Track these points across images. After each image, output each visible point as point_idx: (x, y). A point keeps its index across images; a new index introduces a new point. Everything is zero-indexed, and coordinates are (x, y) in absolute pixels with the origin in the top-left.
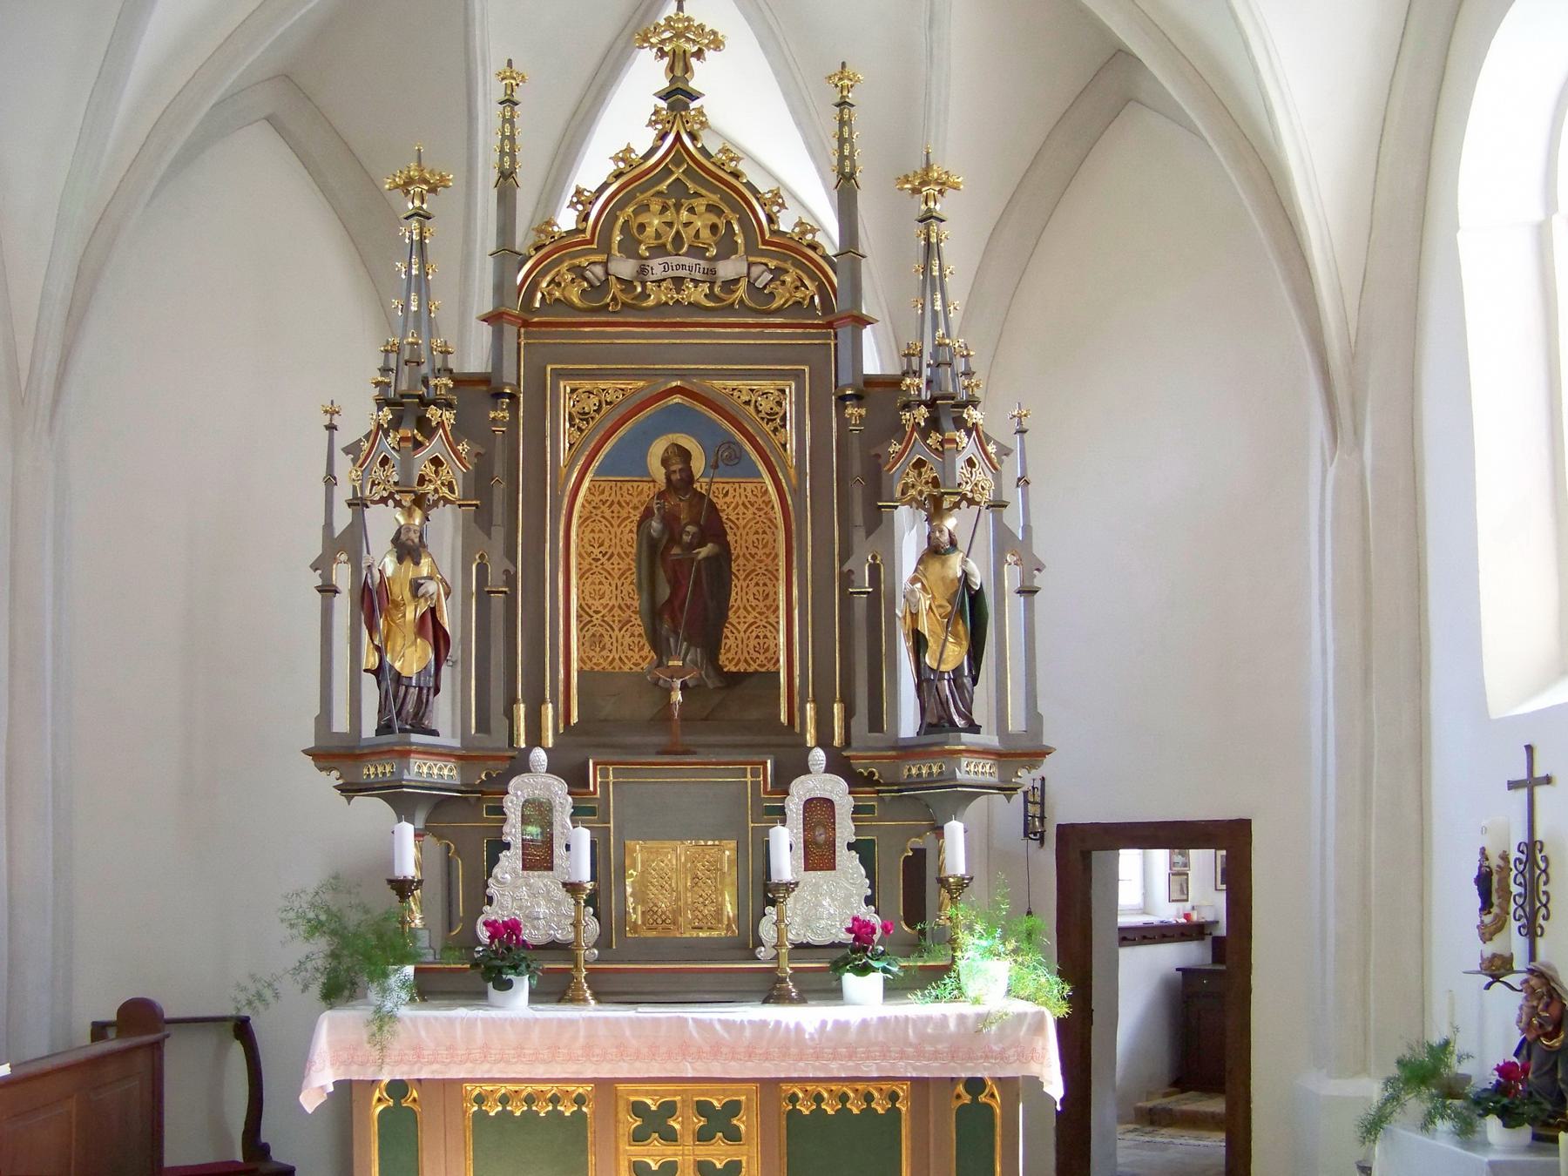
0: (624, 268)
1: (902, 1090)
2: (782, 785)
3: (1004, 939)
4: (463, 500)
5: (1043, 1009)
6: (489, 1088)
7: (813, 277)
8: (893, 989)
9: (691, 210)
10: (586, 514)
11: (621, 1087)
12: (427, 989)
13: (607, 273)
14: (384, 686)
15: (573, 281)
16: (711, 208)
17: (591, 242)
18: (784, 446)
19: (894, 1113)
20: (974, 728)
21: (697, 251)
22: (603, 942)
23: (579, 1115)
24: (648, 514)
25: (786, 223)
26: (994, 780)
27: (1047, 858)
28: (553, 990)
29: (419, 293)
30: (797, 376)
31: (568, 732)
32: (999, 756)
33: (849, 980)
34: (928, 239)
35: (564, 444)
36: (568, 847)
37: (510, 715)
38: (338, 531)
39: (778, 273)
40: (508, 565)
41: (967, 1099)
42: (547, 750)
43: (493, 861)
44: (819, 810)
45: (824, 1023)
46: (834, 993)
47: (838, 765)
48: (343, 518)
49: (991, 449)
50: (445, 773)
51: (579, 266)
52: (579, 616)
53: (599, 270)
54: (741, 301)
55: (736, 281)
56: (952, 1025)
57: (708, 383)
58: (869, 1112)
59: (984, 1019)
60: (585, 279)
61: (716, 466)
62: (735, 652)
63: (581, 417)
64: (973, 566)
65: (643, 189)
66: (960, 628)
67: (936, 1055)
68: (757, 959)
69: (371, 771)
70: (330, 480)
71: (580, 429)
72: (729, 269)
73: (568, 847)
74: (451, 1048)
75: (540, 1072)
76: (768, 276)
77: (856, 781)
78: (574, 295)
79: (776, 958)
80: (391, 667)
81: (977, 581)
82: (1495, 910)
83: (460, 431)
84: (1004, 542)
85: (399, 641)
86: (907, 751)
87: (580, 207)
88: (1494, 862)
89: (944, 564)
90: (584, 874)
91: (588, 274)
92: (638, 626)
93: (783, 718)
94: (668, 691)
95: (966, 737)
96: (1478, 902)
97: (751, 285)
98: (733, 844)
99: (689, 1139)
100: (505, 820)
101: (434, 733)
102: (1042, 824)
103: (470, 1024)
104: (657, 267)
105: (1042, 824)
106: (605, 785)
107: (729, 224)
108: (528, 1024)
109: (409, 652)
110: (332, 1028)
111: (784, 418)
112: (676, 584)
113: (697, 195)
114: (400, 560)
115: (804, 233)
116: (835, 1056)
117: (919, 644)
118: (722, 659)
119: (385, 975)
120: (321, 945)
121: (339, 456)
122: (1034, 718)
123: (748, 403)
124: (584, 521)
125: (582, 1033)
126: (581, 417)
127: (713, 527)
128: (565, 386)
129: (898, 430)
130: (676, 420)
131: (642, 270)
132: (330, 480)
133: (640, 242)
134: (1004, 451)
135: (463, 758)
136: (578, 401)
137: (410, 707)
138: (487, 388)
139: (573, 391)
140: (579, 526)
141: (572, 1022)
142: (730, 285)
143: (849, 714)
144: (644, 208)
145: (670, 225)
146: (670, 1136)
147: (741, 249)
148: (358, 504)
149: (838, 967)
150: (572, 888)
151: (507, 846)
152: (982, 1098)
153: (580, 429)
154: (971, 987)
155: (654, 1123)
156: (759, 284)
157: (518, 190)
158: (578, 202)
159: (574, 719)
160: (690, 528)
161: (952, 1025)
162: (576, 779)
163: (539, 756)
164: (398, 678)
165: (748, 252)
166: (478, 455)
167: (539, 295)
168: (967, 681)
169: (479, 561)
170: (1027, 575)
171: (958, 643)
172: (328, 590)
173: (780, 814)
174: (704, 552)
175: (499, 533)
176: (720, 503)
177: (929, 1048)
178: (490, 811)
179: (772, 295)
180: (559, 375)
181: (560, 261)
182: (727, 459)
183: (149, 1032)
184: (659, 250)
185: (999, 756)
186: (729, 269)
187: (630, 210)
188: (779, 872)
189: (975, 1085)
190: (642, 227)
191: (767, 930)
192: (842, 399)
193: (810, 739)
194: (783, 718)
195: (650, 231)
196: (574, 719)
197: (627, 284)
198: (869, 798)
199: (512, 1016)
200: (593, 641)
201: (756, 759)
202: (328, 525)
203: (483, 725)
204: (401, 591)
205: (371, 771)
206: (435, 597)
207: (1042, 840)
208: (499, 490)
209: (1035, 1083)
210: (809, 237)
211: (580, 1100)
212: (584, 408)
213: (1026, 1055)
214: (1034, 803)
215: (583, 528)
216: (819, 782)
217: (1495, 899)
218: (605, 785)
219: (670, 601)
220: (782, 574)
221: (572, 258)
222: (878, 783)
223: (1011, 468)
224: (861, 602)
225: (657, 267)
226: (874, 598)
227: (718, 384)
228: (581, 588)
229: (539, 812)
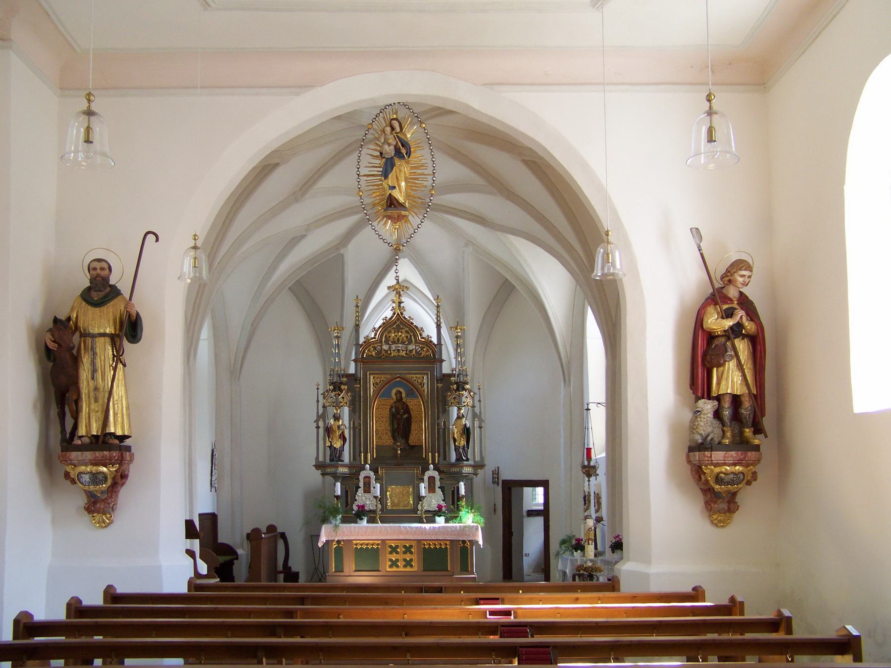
0: (385, 347)
1: (448, 543)
2: (423, 473)
3: (471, 509)
5: (478, 525)
6: (358, 542)
7: (431, 349)
8: (447, 521)
9: (401, 332)
11: (387, 542)
12: (345, 520)
13: (381, 348)
14: (331, 450)
16: (406, 332)
18: (424, 391)
19: (446, 548)
20: (468, 460)
21: (403, 343)
22: (382, 510)
23: (378, 548)
24: (392, 407)
25: (424, 335)
26: (473, 472)
27: (499, 489)
28: (371, 520)
29: (338, 357)
30: (427, 374)
31: (373, 459)
32: (474, 467)
33: (437, 518)
34: (457, 342)
35: (372, 391)
36: (374, 488)
37: (360, 456)
38: (320, 413)
39: (422, 348)
40: (359, 421)
41: (462, 545)
42: (369, 464)
43: (357, 491)
44: (432, 479)
45: (430, 527)
46: (434, 521)
47: (436, 468)
48: (321, 411)
49: (472, 394)
50: (346, 470)
53: (379, 347)
54: (414, 355)
55: (413, 350)
56: (458, 528)
57: (406, 376)
58: (441, 548)
59: (465, 527)
61: (408, 395)
62: (412, 440)
64: (467, 422)
65: (390, 326)
66: (464, 437)
67: (455, 535)
68: (417, 514)
69: (328, 470)
70: (318, 401)
72: (411, 347)
73: (374, 488)
74: (351, 532)
75: (370, 538)
76: (420, 349)
77: (440, 472)
79: (421, 514)
80: (333, 446)
81: (468, 426)
82: (587, 505)
83: (348, 391)
84: (475, 415)
85: (335, 440)
86: (453, 465)
88: (587, 494)
89: (461, 420)
90: (378, 494)
91: (377, 349)
92: (390, 434)
93: (424, 456)
94: (397, 450)
95: (465, 462)
96: (583, 503)
97: (416, 351)
98: (412, 486)
99: (401, 553)
100: (359, 481)
101: (343, 461)
102: (498, 480)
103: (355, 527)
104: (393, 347)
105: (498, 480)
106: (382, 473)
107: (411, 336)
108: (367, 527)
109: (337, 442)
110: (325, 529)
111: (424, 384)
112: (398, 425)
113: (403, 328)
114: (335, 421)
115: (428, 338)
116: (433, 535)
117: (455, 440)
118: (409, 442)
119: (336, 517)
120: (321, 511)
121: (320, 396)
122: (482, 457)
123: (415, 380)
124: (376, 409)
125: (379, 529)
127: (407, 410)
128: (372, 377)
129: (449, 389)
130: (399, 384)
131: (390, 348)
132: (318, 401)
133: (389, 341)
134: (475, 394)
135: (349, 466)
137: (337, 455)
138: (353, 378)
139: (374, 378)
141: (376, 527)
142: (411, 351)
143: (439, 456)
144: (390, 332)
145: (396, 336)
146: (397, 553)
147: (414, 342)
148: (324, 407)
149: (434, 515)
150: (376, 497)
151: (360, 487)
152: (466, 545)
154: (463, 520)
155: (394, 550)
156: (418, 351)
159: (375, 457)
160: (402, 411)
161: (458, 528)
162: (376, 471)
163: (368, 466)
164: (335, 448)
165: (415, 343)
166: (353, 396)
167: (365, 354)
168: (466, 449)
170: (480, 424)
171: (464, 440)
172: (318, 427)
173: (422, 480)
174: (405, 416)
175: (357, 414)
176: (409, 404)
177: (453, 533)
178: (356, 479)
179: (421, 354)
180: (370, 374)
182: (410, 393)
183: (273, 533)
184: (394, 342)
185: (474, 467)
186: (411, 347)
187: (386, 333)
188: (422, 493)
189: (464, 542)
190: (390, 337)
191: (419, 507)
192: (437, 380)
193: (430, 462)
194: (424, 456)
195: (391, 338)
196: (375, 457)
197: (386, 351)
198: (443, 476)
200: (379, 438)
201: (417, 467)
202: (318, 412)
203: (354, 459)
204: (335, 428)
205: (328, 470)
207: (498, 484)
208: (357, 404)
209: (477, 542)
210: (430, 339)
211: (378, 545)
213: (475, 535)
214: (496, 474)
216: (431, 472)
217: (587, 503)
218: (382, 473)
219: (397, 428)
220: (423, 422)
222: (445, 473)
223: (477, 398)
224: (441, 430)
225: (393, 347)
226: (444, 429)
227: (408, 376)
229: (367, 478)
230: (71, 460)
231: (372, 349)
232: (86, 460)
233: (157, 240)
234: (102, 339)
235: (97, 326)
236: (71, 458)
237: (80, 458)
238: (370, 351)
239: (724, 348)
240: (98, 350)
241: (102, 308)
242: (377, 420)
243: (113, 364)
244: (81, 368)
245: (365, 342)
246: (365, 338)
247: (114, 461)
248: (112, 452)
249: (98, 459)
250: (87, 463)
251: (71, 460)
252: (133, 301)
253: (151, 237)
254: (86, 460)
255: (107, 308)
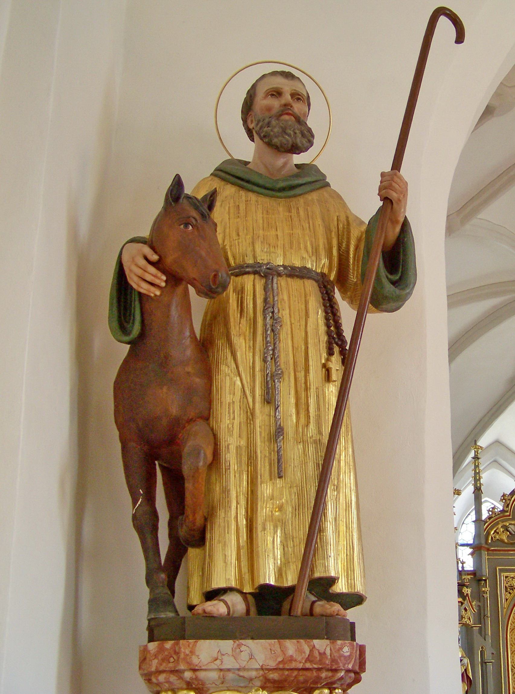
4: (474, 624)
10: (512, 627)
15: (503, 532)
17: (509, 516)
51: (505, 525)
52: (512, 670)
60: (508, 531)
63: (510, 588)
71: (510, 593)
78: (504, 538)
87: (491, 513)
126: (510, 588)
136: (508, 581)
140: (510, 632)
153: (510, 593)
157: (482, 495)
158: (504, 499)
169: (481, 649)
180: (501, 571)
181: (498, 523)
199: (335, 296)
206: (466, 665)
212: (511, 584)
215: (511, 633)
221: (503, 522)
228: (512, 658)
230: (194, 670)
231: (502, 530)
232: (248, 670)
233: (460, 39)
234: (295, 284)
235: (280, 243)
236: (195, 660)
237: (229, 663)
238: (498, 533)
239: (242, 678)
240: (284, 314)
241: (293, 202)
242: (513, 649)
243: (278, 386)
244: (223, 368)
245: (490, 518)
246: (489, 511)
247: (342, 674)
248: (339, 642)
249: (293, 665)
250: (251, 680)
251: (194, 670)
252: (404, 171)
253: (443, 22)
254: (248, 670)
255: (154, 336)
